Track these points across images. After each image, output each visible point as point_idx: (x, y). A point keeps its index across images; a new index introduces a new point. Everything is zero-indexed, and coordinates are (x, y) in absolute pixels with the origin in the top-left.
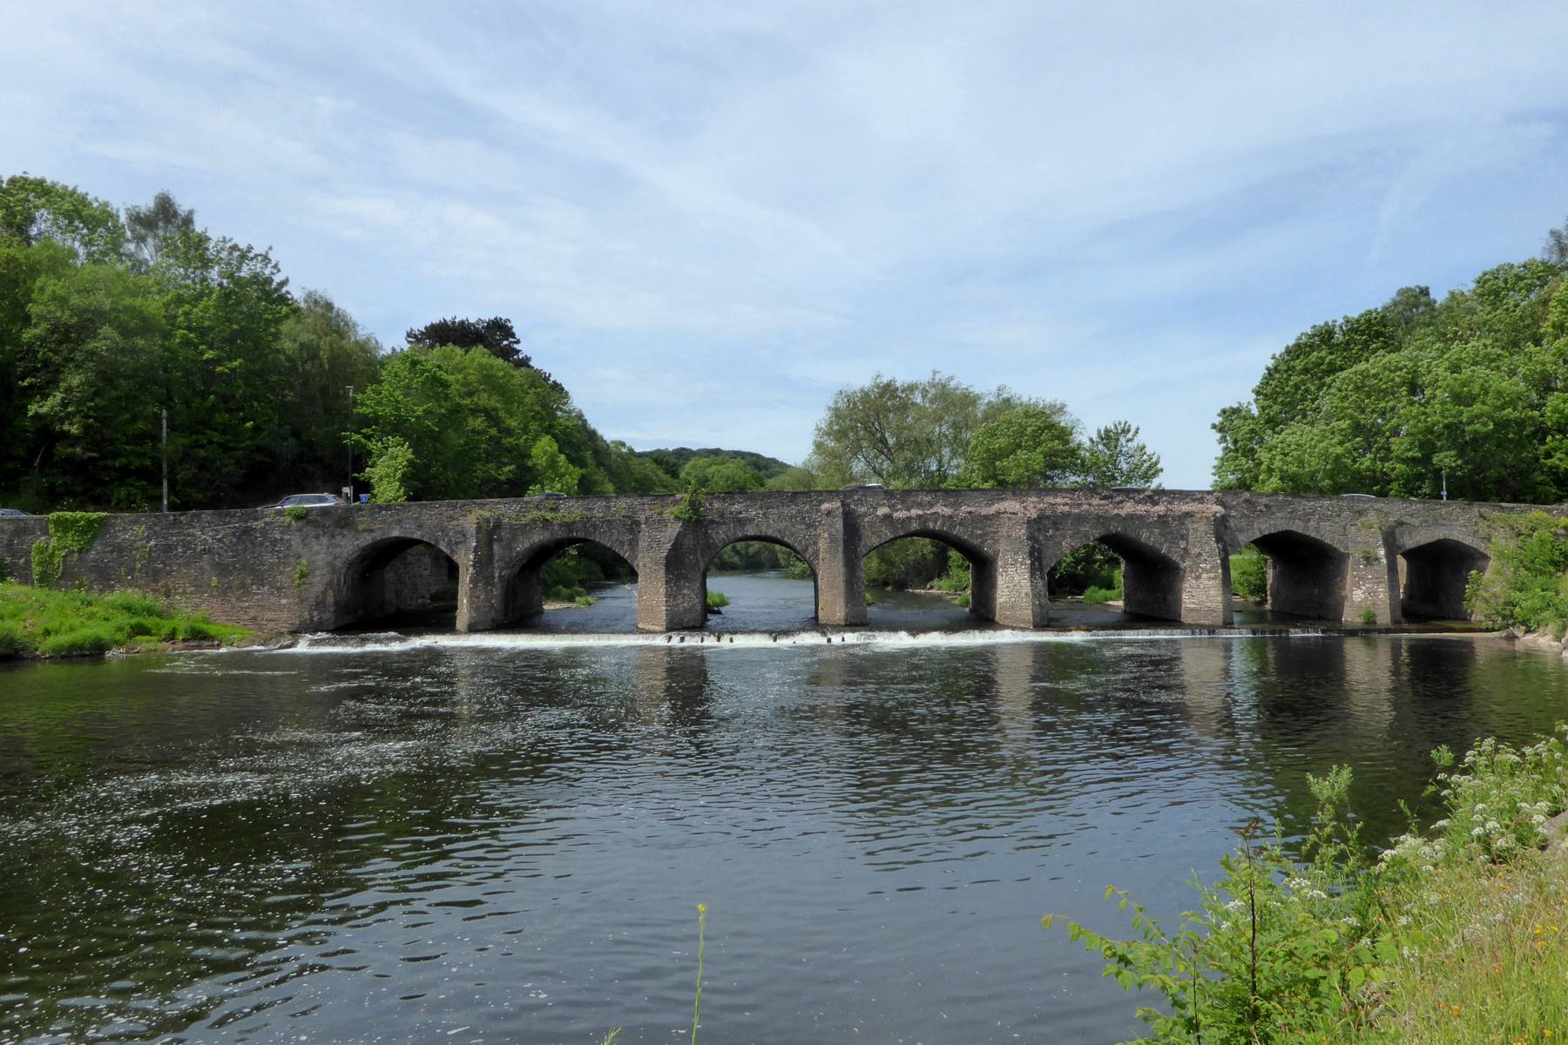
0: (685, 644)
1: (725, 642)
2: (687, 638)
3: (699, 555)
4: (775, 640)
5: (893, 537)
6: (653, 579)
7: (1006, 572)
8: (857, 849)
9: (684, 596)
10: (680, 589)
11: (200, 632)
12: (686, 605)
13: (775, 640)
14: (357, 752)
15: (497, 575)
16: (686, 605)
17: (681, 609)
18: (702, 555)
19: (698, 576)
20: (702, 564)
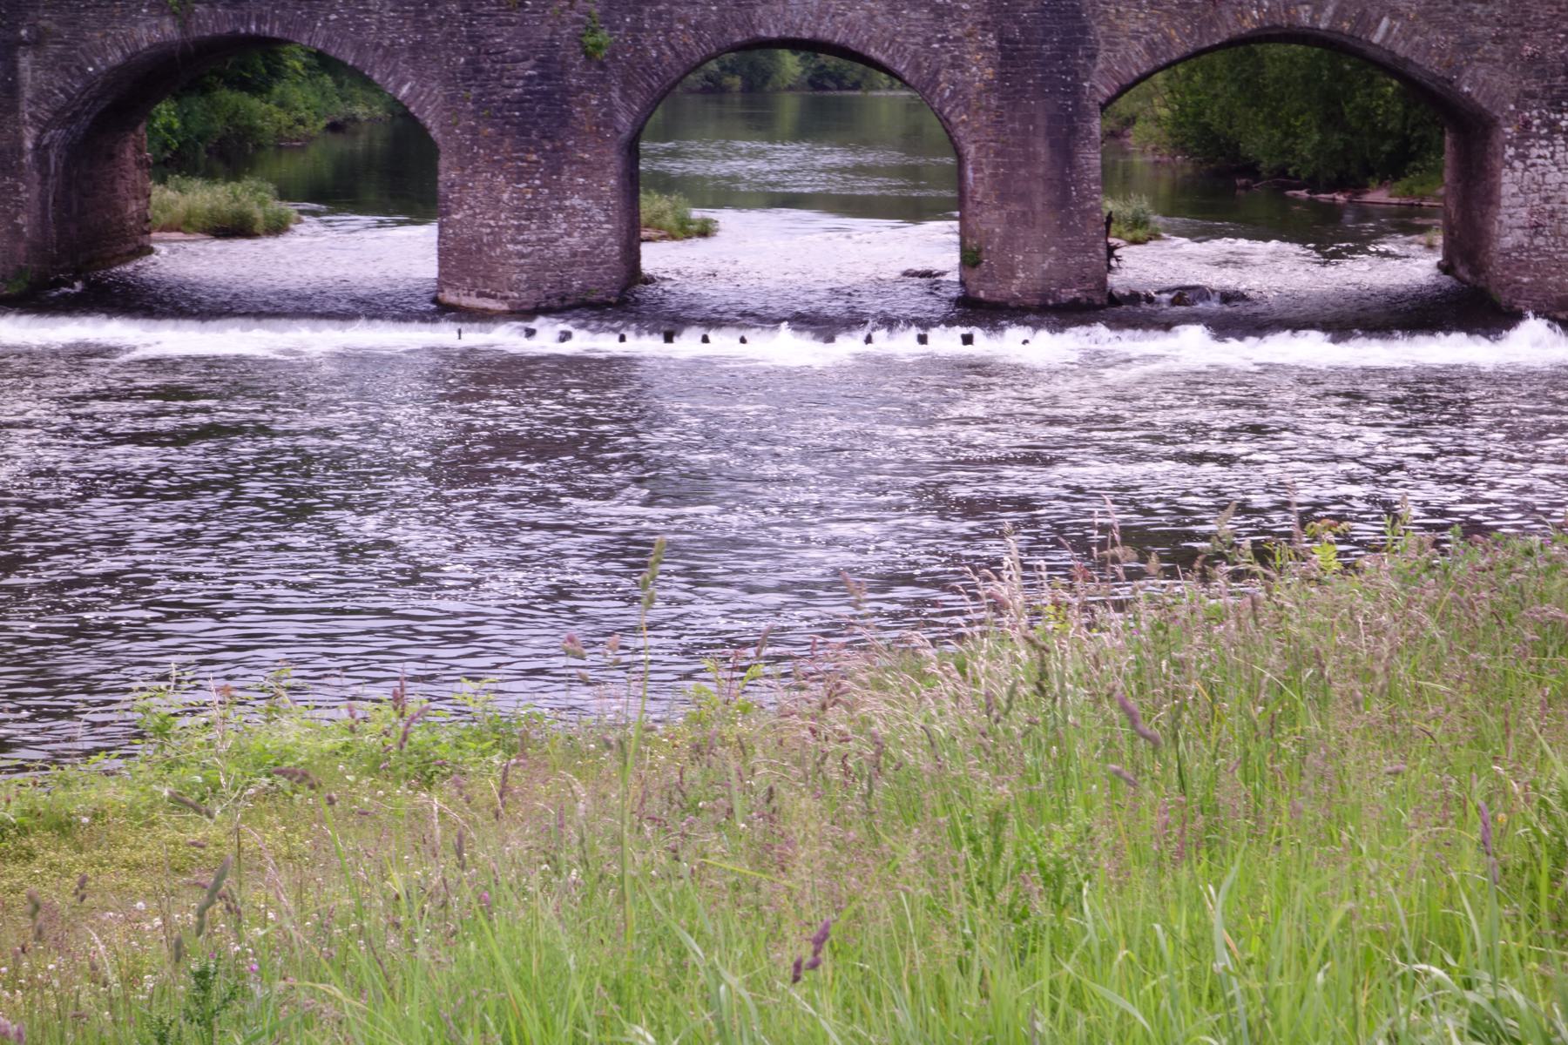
0: (567, 348)
1: (688, 345)
2: (630, 336)
3: (615, 95)
4: (669, 338)
5: (1190, 47)
6: (480, 163)
7: (1523, 157)
8: (142, 726)
9: (570, 214)
10: (559, 193)
11: (1222, 465)
12: (575, 240)
13: (669, 338)
14: (581, 806)
15: (29, 144)
16: (575, 240)
17: (564, 251)
18: (625, 96)
19: (614, 160)
20: (624, 120)
